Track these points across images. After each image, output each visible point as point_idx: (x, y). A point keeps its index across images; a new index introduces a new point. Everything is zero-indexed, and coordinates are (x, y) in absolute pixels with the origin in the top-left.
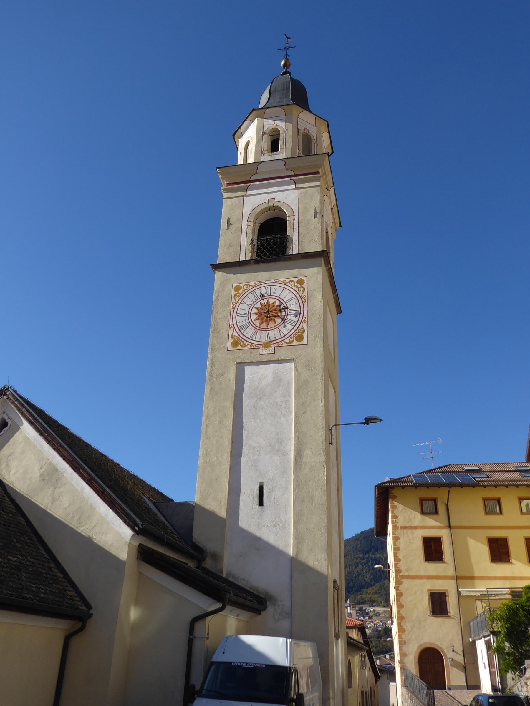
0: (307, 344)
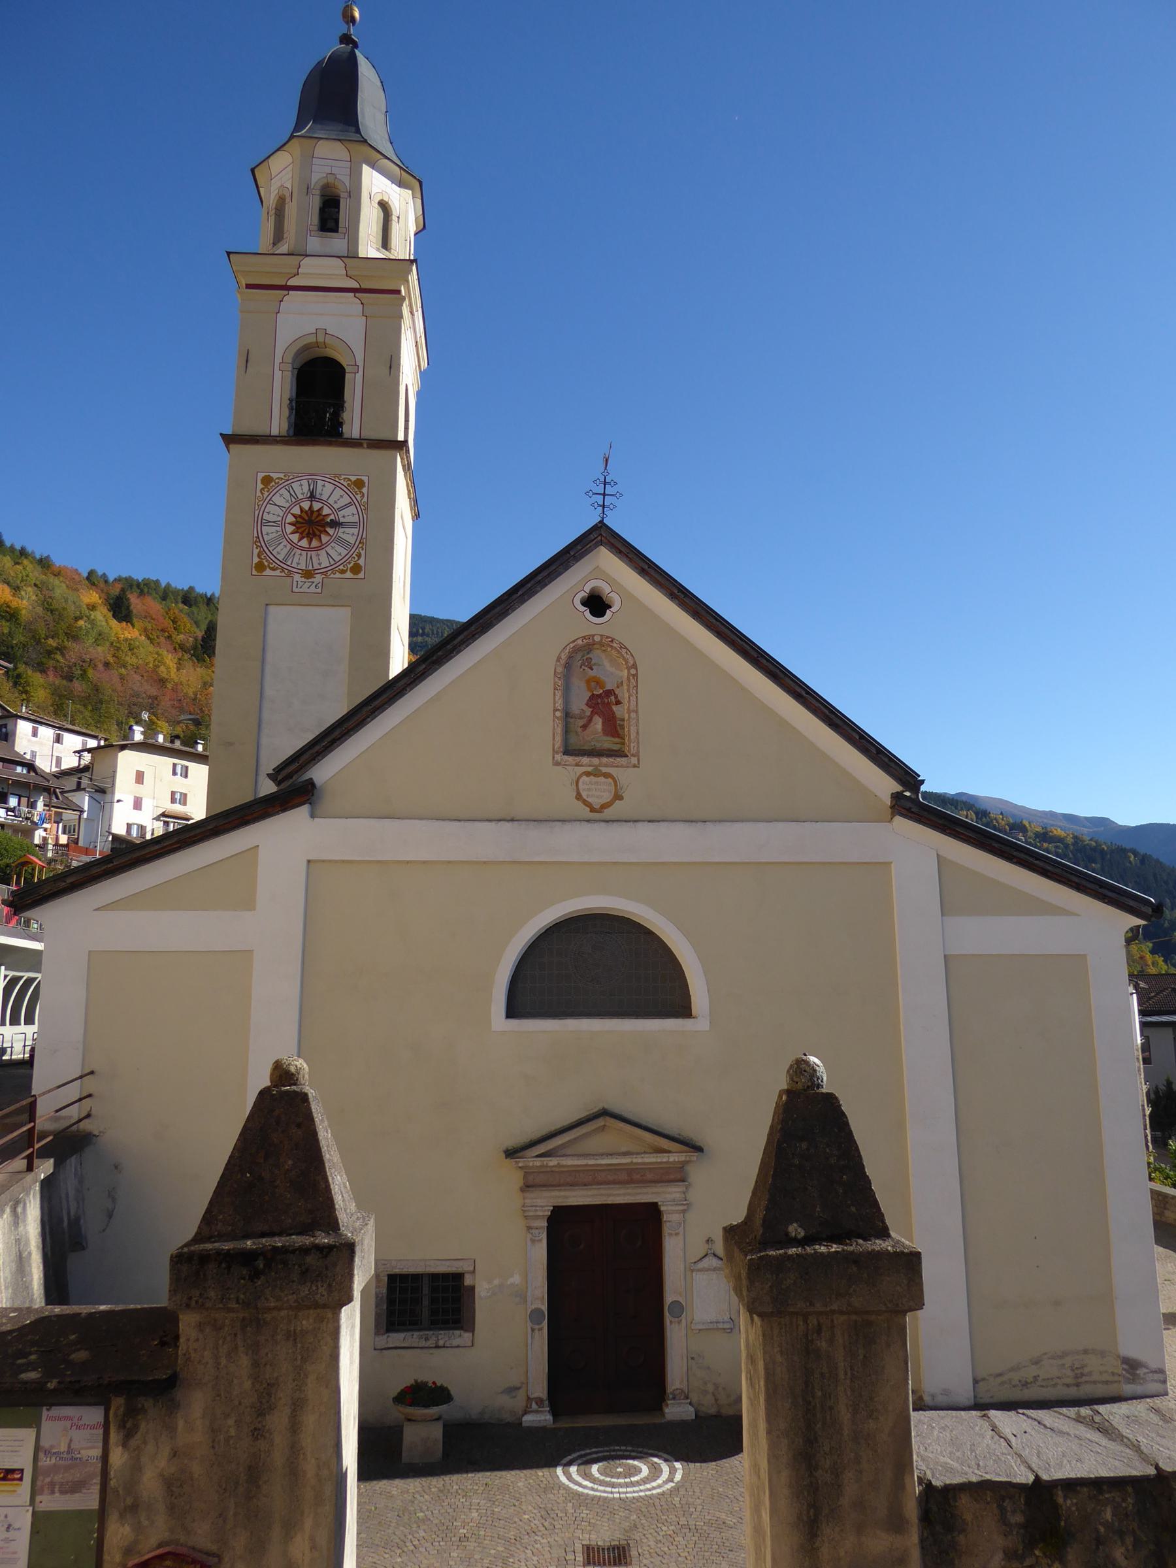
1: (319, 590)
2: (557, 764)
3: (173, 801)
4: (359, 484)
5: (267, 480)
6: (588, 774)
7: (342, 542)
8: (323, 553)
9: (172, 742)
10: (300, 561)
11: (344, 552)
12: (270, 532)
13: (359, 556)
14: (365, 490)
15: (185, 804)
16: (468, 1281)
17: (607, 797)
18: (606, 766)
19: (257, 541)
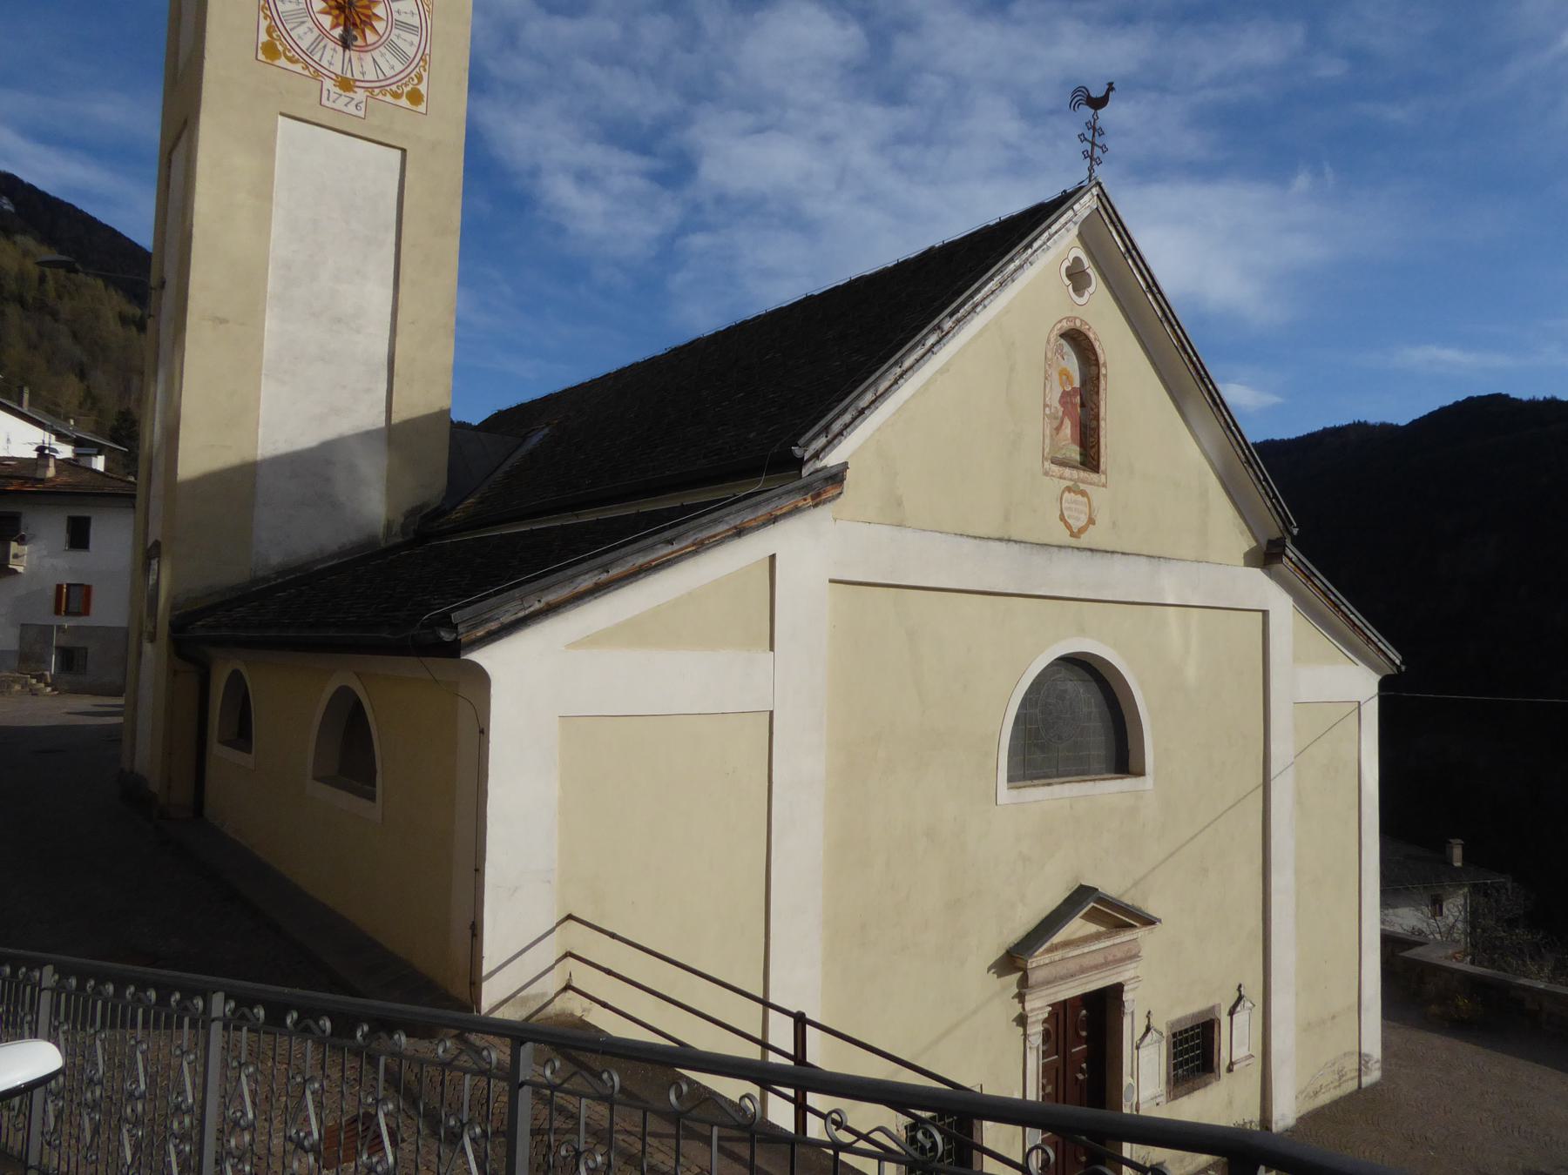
0: (1091, 521)
1: (361, 114)
2: (1046, 474)
6: (1069, 489)
8: (368, 57)
10: (333, 57)
11: (399, 67)
13: (420, 79)
18: (1083, 482)
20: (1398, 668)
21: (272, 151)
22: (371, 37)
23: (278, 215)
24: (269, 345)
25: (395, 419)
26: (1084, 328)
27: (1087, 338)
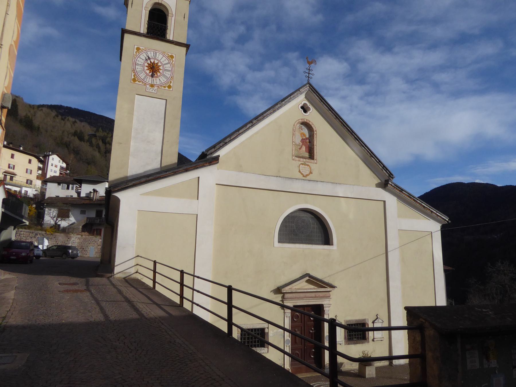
2: (293, 160)
3: (9, 167)
4: (172, 57)
5: (138, 49)
6: (302, 164)
7: (165, 76)
8: (158, 79)
9: (9, 145)
10: (149, 80)
12: (139, 68)
13: (171, 82)
14: (174, 59)
15: (14, 169)
16: (266, 331)
17: (308, 172)
19: (134, 70)
20: (448, 222)
21: (134, 103)
22: (159, 74)
23: (135, 118)
24: (132, 149)
25: (163, 165)
26: (308, 122)
27: (309, 124)
